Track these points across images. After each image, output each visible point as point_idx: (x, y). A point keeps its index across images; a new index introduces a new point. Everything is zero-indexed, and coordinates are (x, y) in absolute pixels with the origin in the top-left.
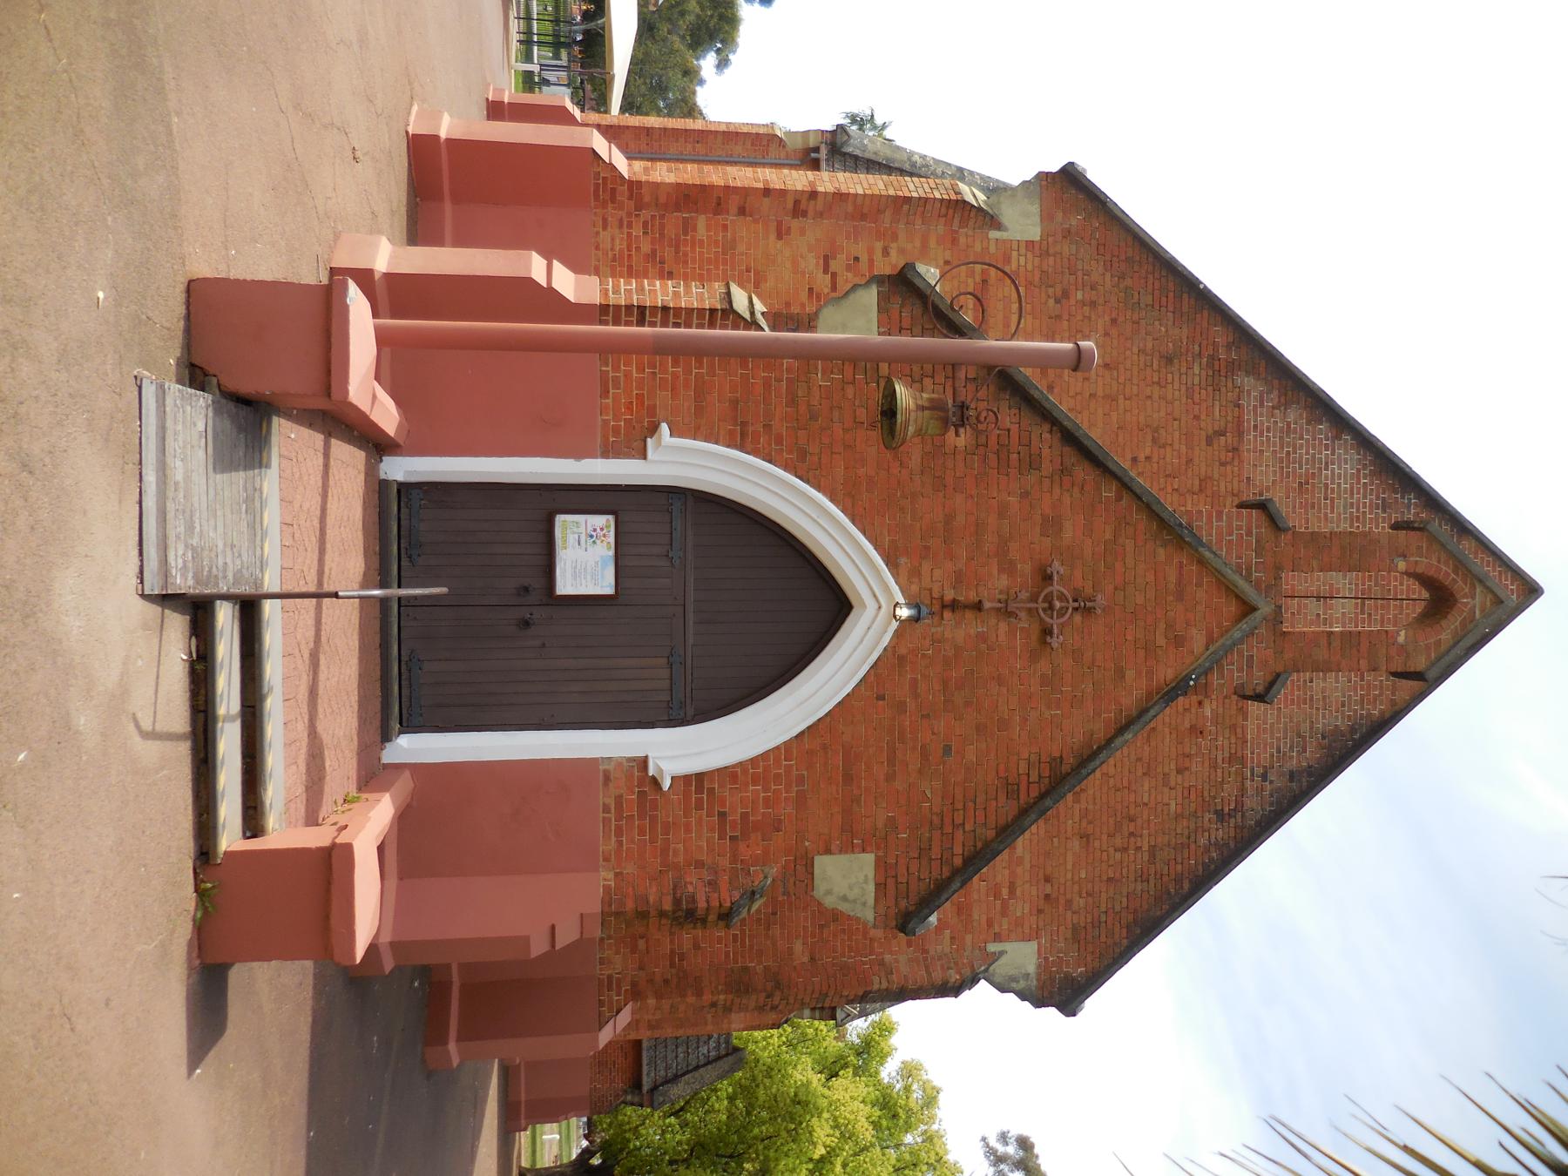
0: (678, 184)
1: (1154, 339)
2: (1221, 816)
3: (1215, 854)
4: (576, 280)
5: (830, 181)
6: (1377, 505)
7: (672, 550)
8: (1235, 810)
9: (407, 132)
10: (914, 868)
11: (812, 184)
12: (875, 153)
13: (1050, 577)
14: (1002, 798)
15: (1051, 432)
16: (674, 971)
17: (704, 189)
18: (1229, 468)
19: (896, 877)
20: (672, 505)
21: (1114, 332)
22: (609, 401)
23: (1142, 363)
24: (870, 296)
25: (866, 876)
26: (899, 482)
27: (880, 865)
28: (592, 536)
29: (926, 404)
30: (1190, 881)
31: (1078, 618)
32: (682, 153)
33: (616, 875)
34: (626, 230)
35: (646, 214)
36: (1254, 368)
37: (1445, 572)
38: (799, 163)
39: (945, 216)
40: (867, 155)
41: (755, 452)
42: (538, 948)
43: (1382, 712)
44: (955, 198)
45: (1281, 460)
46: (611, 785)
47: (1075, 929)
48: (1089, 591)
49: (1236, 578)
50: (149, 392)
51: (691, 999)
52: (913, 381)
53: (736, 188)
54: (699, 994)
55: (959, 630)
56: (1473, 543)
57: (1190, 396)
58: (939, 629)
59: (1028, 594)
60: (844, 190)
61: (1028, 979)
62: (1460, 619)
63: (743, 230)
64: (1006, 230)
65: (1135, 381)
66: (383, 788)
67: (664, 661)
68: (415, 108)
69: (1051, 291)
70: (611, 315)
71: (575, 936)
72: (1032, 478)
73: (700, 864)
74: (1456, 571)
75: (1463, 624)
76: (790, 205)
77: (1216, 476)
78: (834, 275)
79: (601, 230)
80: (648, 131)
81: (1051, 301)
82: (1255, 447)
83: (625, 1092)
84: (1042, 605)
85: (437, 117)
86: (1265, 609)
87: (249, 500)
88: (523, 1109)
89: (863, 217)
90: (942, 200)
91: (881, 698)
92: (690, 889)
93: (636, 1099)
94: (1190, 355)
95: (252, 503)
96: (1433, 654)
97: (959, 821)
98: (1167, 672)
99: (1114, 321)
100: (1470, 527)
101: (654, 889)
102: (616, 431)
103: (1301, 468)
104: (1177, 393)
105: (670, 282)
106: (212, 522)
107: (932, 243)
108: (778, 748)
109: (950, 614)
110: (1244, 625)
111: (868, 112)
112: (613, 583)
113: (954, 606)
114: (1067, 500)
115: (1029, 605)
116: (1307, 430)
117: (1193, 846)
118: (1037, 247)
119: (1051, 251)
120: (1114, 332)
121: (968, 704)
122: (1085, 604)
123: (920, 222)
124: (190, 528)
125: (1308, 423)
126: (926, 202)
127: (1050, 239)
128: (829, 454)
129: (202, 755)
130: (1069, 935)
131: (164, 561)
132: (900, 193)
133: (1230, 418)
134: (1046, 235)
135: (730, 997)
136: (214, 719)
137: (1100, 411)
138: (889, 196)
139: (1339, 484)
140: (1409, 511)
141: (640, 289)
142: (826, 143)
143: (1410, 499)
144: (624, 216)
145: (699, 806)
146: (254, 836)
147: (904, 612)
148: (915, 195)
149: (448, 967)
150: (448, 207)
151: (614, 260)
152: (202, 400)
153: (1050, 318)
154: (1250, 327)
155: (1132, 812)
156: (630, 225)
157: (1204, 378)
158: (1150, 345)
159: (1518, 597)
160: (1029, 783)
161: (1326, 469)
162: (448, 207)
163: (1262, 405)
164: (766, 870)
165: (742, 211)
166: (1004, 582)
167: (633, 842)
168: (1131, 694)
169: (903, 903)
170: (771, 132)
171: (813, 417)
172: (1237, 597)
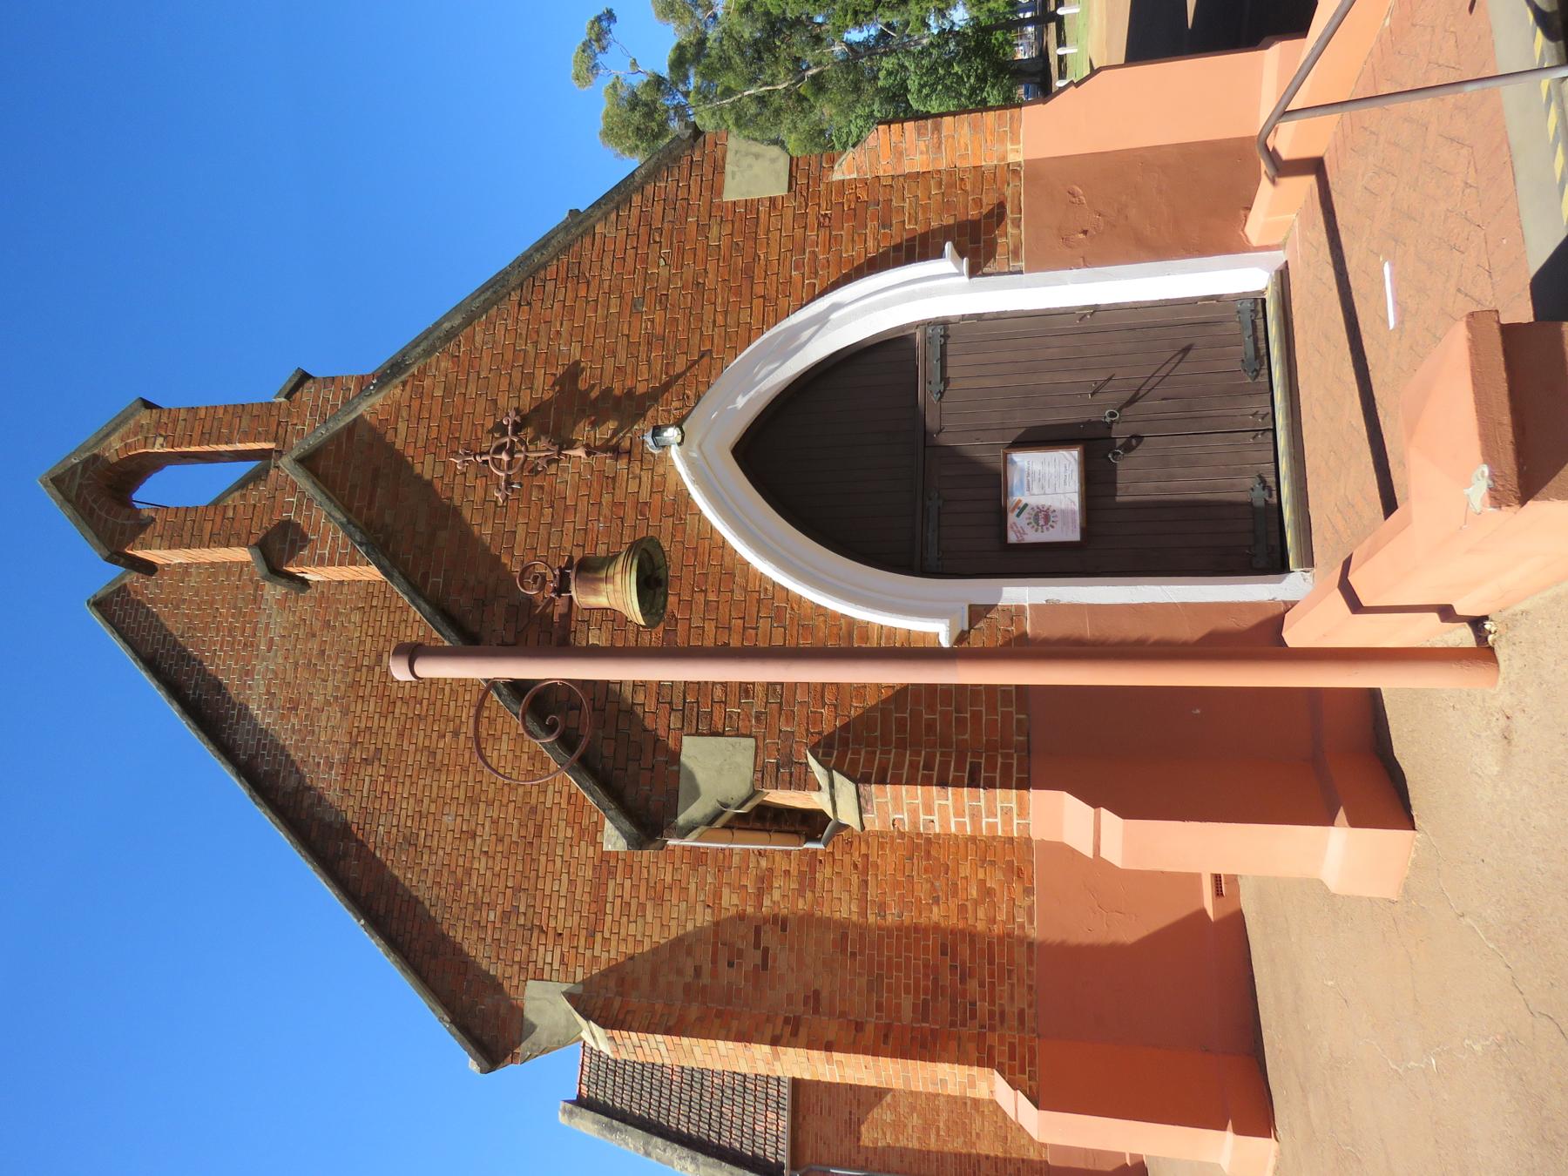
0: (933, 1060)
7: (939, 508)
11: (776, 1057)
20: (939, 559)
25: (733, 178)
27: (716, 188)
39: (628, 1012)
43: (256, 487)
53: (865, 1052)
64: (564, 994)
69: (522, 921)
70: (1014, 779)
76: (803, 1031)
90: (629, 1029)
105: (937, 831)
116: (280, 765)
122: (475, 459)
125: (278, 772)
126: (648, 1027)
128: (747, 618)
132: (676, 1039)
133: (355, 777)
140: (196, 682)
141: (976, 816)
143: (194, 693)
151: (1010, 972)
156: (992, 1015)
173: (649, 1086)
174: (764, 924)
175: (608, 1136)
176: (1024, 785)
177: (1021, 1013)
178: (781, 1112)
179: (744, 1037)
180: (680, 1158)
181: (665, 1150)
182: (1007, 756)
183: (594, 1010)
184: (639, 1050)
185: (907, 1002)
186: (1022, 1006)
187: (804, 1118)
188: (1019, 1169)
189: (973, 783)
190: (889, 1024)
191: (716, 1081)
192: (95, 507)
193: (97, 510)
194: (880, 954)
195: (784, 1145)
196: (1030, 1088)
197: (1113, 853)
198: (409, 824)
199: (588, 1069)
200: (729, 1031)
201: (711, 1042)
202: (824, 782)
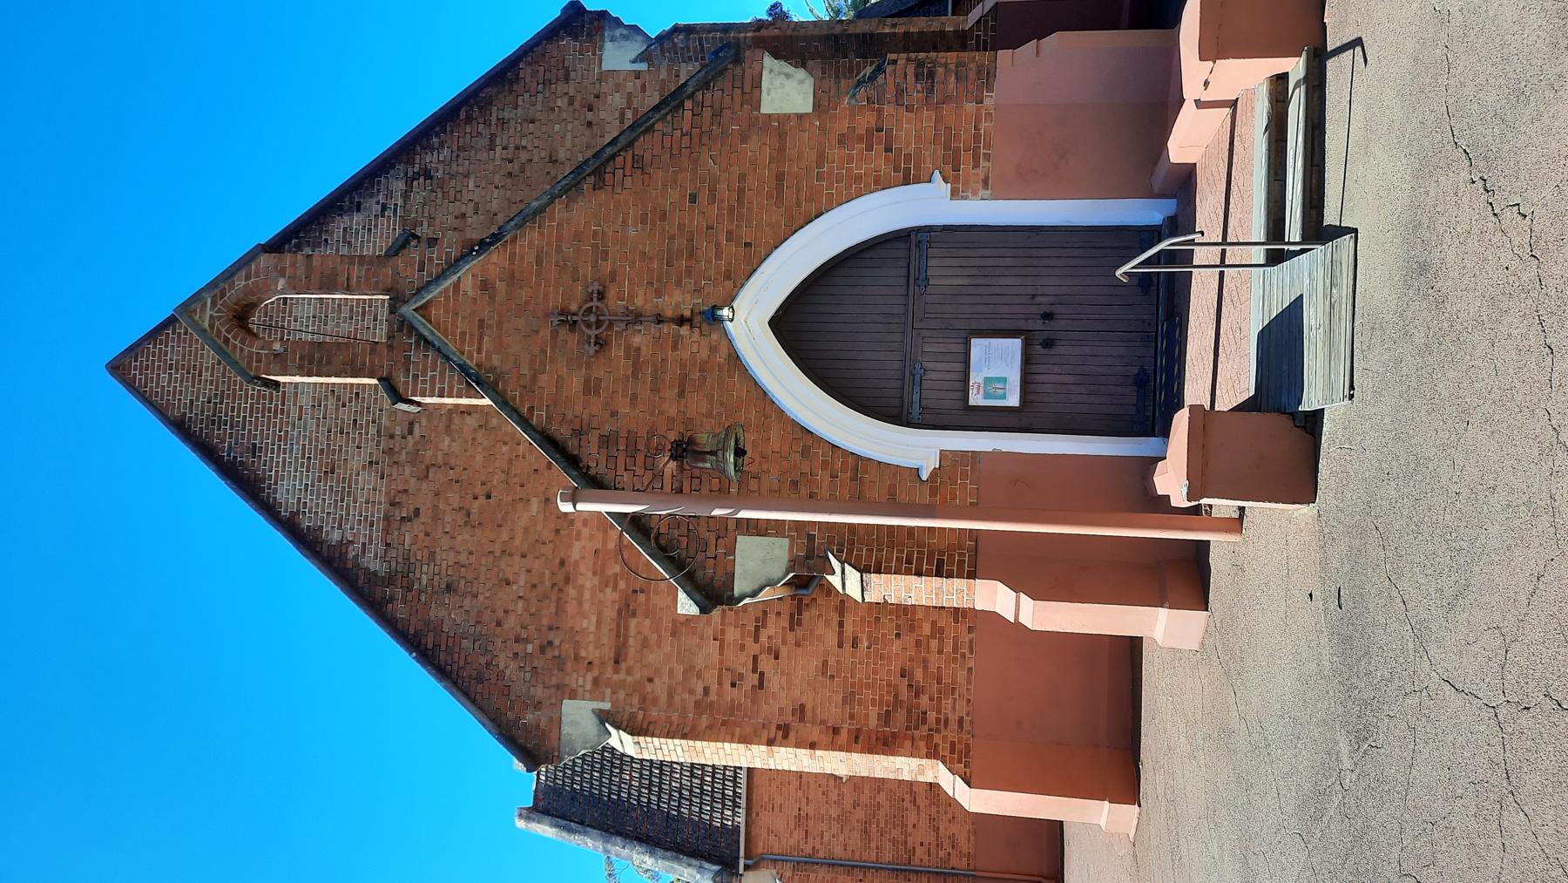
2: (427, 174)
3: (434, 140)
8: (414, 179)
9: (1140, 806)
10: (727, 100)
14: (647, 157)
15: (588, 467)
17: (870, 750)
18: (400, 488)
19: (743, 93)
25: (769, 95)
29: (708, 456)
30: (458, 116)
33: (981, 102)
39: (650, 723)
44: (640, 738)
47: (567, 79)
55: (678, 300)
57: (432, 555)
58: (696, 301)
61: (612, 37)
62: (226, 298)
63: (834, 712)
64: (593, 711)
67: (930, 282)
69: (556, 653)
72: (607, 429)
73: (909, 109)
76: (792, 735)
77: (413, 481)
81: (557, 642)
82: (373, 506)
90: (653, 735)
91: (746, 245)
92: (919, 86)
96: (253, 267)
97: (686, 138)
98: (495, 259)
99: (499, 624)
101: (951, 87)
102: (964, 475)
107: (663, 699)
109: (685, 314)
113: (681, 321)
117: (455, 148)
120: (501, 614)
123: (673, 718)
130: (573, 75)
132: (691, 743)
143: (229, 455)
147: (726, 312)
155: (509, 181)
156: (938, 721)
157: (418, 571)
160: (623, 169)
166: (637, 340)
168: (529, 241)
169: (738, 70)
174: (761, 654)
175: (567, 837)
176: (972, 575)
179: (746, 740)
180: (638, 854)
182: (962, 555)
183: (622, 723)
184: (659, 752)
185: (873, 712)
186: (961, 715)
187: (757, 814)
189: (939, 574)
190: (859, 729)
192: (229, 336)
193: (231, 340)
196: (965, 773)
197: (1027, 619)
199: (543, 778)
201: (719, 744)
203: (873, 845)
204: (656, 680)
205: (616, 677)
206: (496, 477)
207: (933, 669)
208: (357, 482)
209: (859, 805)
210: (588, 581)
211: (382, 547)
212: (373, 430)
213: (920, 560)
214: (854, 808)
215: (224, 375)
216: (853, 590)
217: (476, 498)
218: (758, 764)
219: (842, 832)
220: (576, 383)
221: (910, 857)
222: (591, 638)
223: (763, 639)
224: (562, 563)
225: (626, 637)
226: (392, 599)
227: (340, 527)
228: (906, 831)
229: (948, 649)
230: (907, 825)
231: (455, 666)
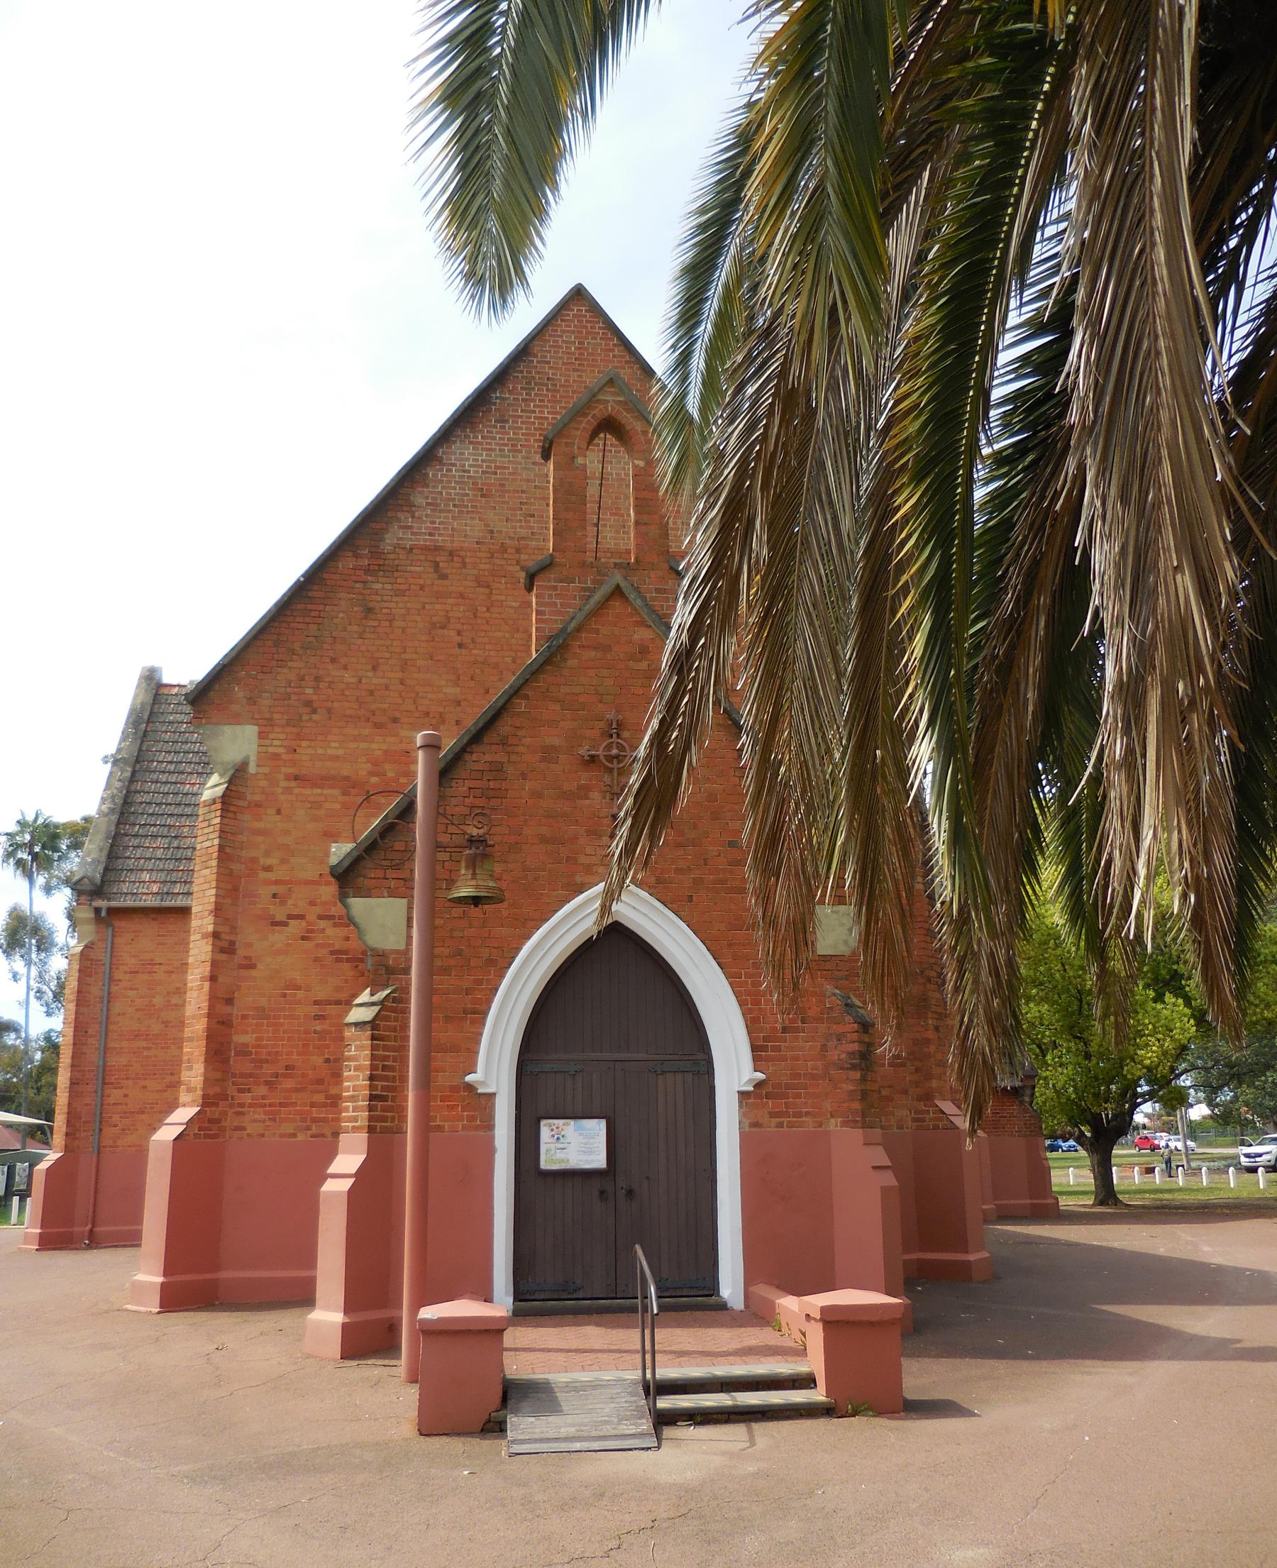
0: (206, 1061)
1: (350, 624)
4: (343, 1153)
5: (202, 918)
6: (502, 427)
9: (159, 1313)
12: (101, 850)
13: (592, 756)
15: (472, 753)
16: (909, 1064)
17: (211, 1037)
18: (468, 560)
21: (343, 660)
22: (447, 1125)
23: (372, 636)
24: (358, 905)
26: (513, 881)
28: (558, 1139)
29: (471, 872)
31: (626, 734)
32: (98, 1049)
33: (832, 1116)
34: (246, 1109)
35: (232, 1091)
36: (376, 534)
37: (587, 423)
38: (110, 929)
39: (235, 813)
40: (104, 859)
41: (489, 1002)
42: (889, 1179)
45: (462, 512)
46: (761, 1121)
48: (602, 724)
49: (593, 602)
50: (517, 1448)
51: (932, 1048)
52: (451, 883)
54: (927, 1041)
56: (535, 342)
57: (402, 593)
59: (606, 776)
60: (212, 907)
63: (247, 1000)
64: (247, 757)
65: (389, 643)
66: (771, 1306)
67: (660, 1078)
68: (129, 1307)
69: (305, 717)
71: (880, 1150)
72: (510, 770)
73: (824, 1048)
74: (586, 415)
75: (629, 411)
76: (223, 957)
77: (476, 572)
78: (291, 917)
79: (245, 1132)
80: (74, 1083)
81: (315, 717)
83: (1022, 1102)
84: (615, 765)
85: (139, 1288)
86: (617, 578)
87: (576, 1390)
88: (1036, 1201)
89: (236, 889)
90: (221, 816)
92: (843, 1056)
93: (1028, 1092)
94: (365, 592)
95: (576, 1388)
99: (333, 660)
100: (522, 345)
103: (468, 495)
104: (400, 605)
106: (599, 1411)
108: (731, 984)
110: (632, 596)
111: (4, 838)
112: (596, 1121)
114: (528, 741)
115: (615, 774)
116: (434, 487)
118: (264, 729)
119: (267, 716)
120: (343, 660)
121: (695, 827)
124: (606, 1423)
125: (427, 486)
127: (257, 716)
129: (760, 1416)
131: (633, 1436)
132: (215, 855)
134: (253, 721)
135: (930, 1015)
136: (736, 1407)
137: (415, 675)
138: (218, 866)
139: (482, 461)
140: (507, 399)
141: (353, 1099)
142: (91, 900)
143: (497, 398)
144: (232, 1110)
145: (778, 1049)
146: (814, 1381)
148: (216, 842)
149: (905, 1262)
150: (223, 1275)
151: (273, 1120)
152: (512, 1420)
153: (330, 718)
154: (340, 537)
158: (355, 628)
159: (584, 305)
161: (469, 472)
162: (223, 1275)
163: (410, 527)
164: (828, 994)
165: (230, 1001)
166: (596, 795)
167: (806, 1103)
170: (77, 957)
171: (459, 953)
172: (608, 600)
173: (179, 759)
176: (371, 1130)
177: (243, 1129)
178: (159, 898)
181: (120, 780)
188: (115, 1126)
191: (186, 830)
192: (589, 418)
194: (285, 1017)
195: (129, 903)
197: (330, 1186)
198: (384, 611)
200: (223, 897)
202: (375, 998)
203: (125, 1044)
204: (278, 817)
205: (282, 777)
206: (481, 652)
207: (294, 1097)
208: (472, 518)
209: (166, 1026)
210: (378, 746)
211: (408, 544)
212: (523, 532)
213: (386, 1078)
214: (163, 1022)
215: (574, 392)
216: (357, 1015)
217: (459, 633)
218: (195, 923)
219: (137, 1010)
220: (553, 739)
221: (112, 1084)
222: (320, 751)
223: (323, 924)
224: (395, 720)
225: (322, 787)
226: (357, 556)
227: (428, 504)
228: (140, 1079)
229: (315, 1113)
230: (145, 1079)
231: (291, 619)
